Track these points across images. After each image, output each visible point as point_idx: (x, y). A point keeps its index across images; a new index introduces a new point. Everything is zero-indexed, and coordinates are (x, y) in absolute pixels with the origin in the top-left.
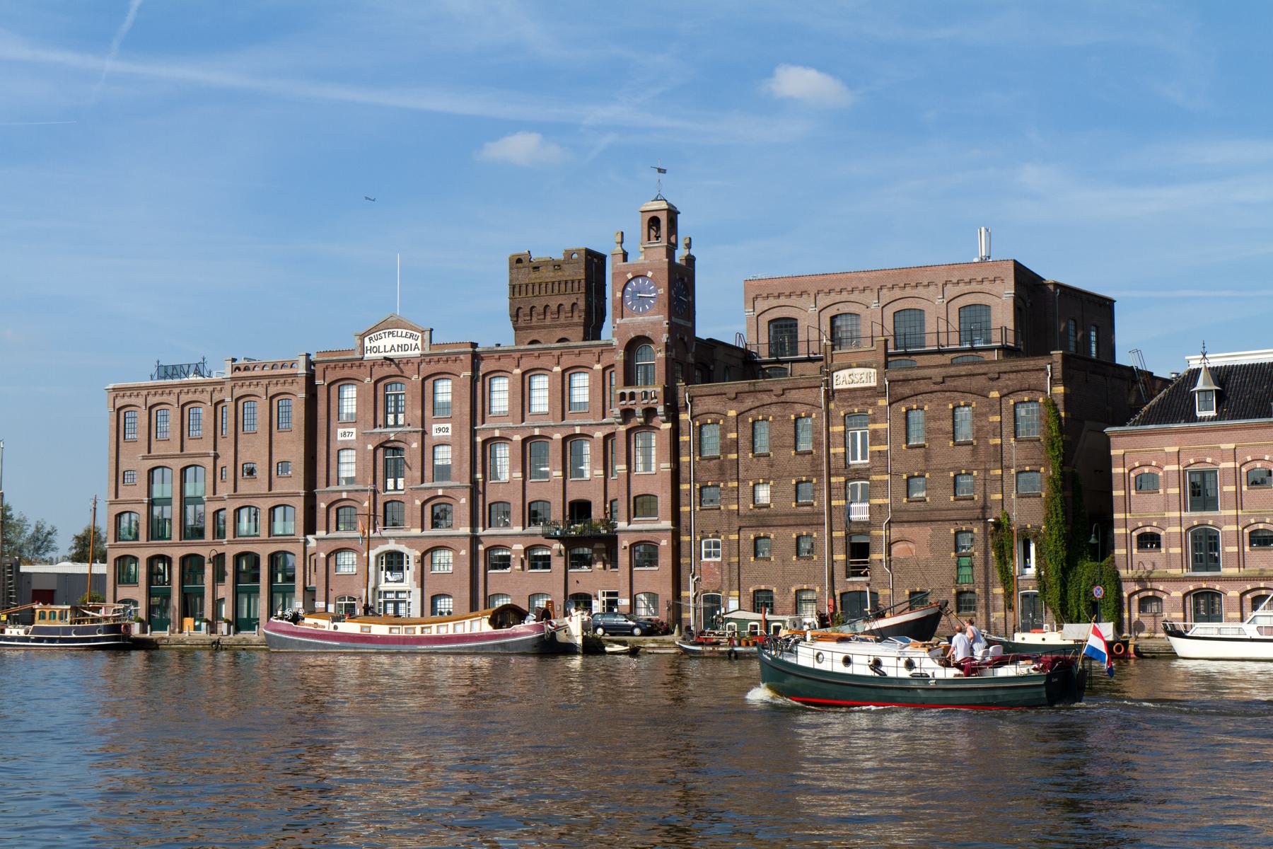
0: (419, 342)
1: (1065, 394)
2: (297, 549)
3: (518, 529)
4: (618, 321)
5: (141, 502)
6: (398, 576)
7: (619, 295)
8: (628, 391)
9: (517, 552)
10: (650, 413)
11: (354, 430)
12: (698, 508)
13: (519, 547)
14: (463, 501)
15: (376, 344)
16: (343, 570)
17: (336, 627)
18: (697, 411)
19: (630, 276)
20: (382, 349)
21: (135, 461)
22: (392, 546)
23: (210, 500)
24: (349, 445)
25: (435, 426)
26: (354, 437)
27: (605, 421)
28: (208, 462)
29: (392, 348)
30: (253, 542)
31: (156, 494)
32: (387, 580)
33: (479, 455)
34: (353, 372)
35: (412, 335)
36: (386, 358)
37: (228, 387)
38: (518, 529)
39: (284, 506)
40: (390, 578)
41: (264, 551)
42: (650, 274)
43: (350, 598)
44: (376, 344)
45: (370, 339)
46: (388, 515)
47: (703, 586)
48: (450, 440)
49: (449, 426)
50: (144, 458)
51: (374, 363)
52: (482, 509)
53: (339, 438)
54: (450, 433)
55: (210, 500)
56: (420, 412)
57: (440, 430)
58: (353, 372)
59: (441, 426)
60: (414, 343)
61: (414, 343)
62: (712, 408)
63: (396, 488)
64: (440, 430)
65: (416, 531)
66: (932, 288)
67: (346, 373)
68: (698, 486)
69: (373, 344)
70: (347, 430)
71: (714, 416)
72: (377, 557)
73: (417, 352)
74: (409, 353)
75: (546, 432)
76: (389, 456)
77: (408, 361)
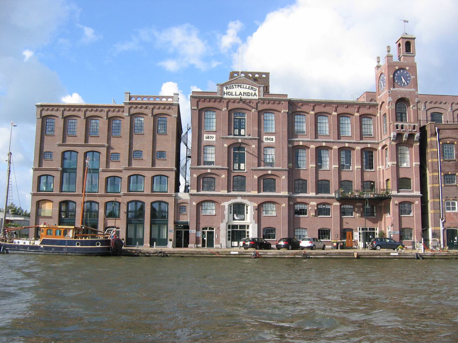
0: (257, 92)
1: (419, 145)
2: (171, 201)
3: (313, 194)
4: (392, 89)
5: (57, 170)
6: (242, 217)
7: (392, 76)
8: (400, 124)
9: (312, 206)
10: (411, 136)
11: (214, 136)
12: (443, 185)
13: (314, 203)
14: (284, 177)
15: (230, 90)
16: (208, 212)
17: (171, 240)
18: (441, 137)
19: (397, 68)
20: (234, 94)
21: (53, 145)
22: (239, 200)
23: (104, 171)
24: (211, 144)
25: (264, 137)
26: (214, 139)
27: (361, 141)
28: (103, 151)
29: (240, 94)
30: (95, 196)
31: (66, 166)
32: (234, 219)
33: (294, 152)
34: (216, 105)
35: (252, 88)
36: (241, 99)
37: (127, 108)
38: (313, 194)
39: (47, 175)
40: (236, 218)
41: (148, 201)
42: (407, 68)
43: (210, 228)
44: (230, 90)
45: (227, 88)
46: (238, 183)
47: (445, 224)
48: (274, 145)
49: (274, 137)
50: (60, 145)
51: (229, 100)
52: (296, 184)
53: (205, 139)
54: (274, 141)
55: (104, 171)
56: (256, 129)
57: (268, 139)
58: (216, 105)
59: (269, 137)
60: (253, 92)
61: (253, 92)
62: (450, 136)
63: (239, 169)
64: (268, 139)
65: (255, 193)
66: (103, 112)
67: (211, 104)
68: (442, 174)
69: (228, 91)
70: (210, 135)
71: (450, 139)
72: (230, 206)
73: (256, 97)
74: (251, 97)
75: (351, 146)
76: (236, 152)
77: (250, 101)
